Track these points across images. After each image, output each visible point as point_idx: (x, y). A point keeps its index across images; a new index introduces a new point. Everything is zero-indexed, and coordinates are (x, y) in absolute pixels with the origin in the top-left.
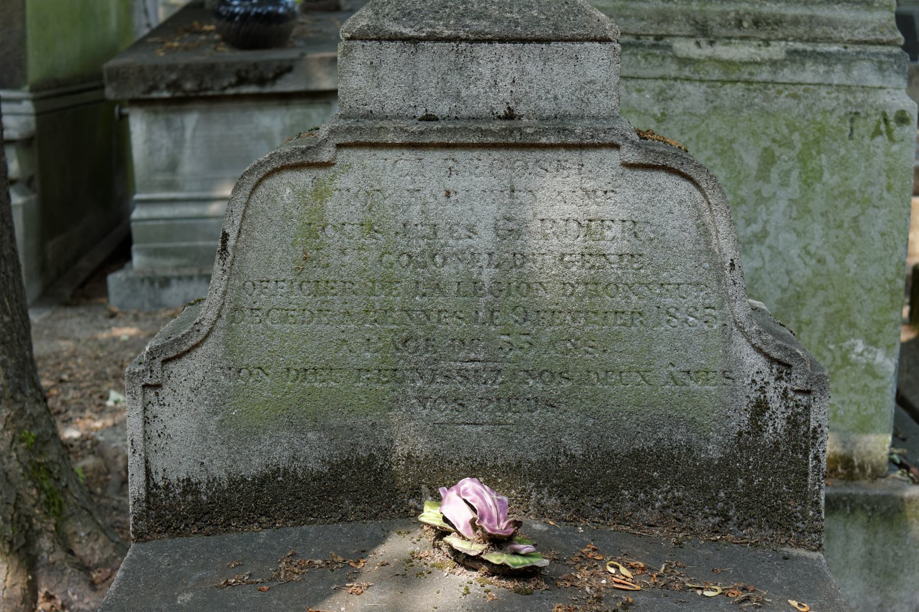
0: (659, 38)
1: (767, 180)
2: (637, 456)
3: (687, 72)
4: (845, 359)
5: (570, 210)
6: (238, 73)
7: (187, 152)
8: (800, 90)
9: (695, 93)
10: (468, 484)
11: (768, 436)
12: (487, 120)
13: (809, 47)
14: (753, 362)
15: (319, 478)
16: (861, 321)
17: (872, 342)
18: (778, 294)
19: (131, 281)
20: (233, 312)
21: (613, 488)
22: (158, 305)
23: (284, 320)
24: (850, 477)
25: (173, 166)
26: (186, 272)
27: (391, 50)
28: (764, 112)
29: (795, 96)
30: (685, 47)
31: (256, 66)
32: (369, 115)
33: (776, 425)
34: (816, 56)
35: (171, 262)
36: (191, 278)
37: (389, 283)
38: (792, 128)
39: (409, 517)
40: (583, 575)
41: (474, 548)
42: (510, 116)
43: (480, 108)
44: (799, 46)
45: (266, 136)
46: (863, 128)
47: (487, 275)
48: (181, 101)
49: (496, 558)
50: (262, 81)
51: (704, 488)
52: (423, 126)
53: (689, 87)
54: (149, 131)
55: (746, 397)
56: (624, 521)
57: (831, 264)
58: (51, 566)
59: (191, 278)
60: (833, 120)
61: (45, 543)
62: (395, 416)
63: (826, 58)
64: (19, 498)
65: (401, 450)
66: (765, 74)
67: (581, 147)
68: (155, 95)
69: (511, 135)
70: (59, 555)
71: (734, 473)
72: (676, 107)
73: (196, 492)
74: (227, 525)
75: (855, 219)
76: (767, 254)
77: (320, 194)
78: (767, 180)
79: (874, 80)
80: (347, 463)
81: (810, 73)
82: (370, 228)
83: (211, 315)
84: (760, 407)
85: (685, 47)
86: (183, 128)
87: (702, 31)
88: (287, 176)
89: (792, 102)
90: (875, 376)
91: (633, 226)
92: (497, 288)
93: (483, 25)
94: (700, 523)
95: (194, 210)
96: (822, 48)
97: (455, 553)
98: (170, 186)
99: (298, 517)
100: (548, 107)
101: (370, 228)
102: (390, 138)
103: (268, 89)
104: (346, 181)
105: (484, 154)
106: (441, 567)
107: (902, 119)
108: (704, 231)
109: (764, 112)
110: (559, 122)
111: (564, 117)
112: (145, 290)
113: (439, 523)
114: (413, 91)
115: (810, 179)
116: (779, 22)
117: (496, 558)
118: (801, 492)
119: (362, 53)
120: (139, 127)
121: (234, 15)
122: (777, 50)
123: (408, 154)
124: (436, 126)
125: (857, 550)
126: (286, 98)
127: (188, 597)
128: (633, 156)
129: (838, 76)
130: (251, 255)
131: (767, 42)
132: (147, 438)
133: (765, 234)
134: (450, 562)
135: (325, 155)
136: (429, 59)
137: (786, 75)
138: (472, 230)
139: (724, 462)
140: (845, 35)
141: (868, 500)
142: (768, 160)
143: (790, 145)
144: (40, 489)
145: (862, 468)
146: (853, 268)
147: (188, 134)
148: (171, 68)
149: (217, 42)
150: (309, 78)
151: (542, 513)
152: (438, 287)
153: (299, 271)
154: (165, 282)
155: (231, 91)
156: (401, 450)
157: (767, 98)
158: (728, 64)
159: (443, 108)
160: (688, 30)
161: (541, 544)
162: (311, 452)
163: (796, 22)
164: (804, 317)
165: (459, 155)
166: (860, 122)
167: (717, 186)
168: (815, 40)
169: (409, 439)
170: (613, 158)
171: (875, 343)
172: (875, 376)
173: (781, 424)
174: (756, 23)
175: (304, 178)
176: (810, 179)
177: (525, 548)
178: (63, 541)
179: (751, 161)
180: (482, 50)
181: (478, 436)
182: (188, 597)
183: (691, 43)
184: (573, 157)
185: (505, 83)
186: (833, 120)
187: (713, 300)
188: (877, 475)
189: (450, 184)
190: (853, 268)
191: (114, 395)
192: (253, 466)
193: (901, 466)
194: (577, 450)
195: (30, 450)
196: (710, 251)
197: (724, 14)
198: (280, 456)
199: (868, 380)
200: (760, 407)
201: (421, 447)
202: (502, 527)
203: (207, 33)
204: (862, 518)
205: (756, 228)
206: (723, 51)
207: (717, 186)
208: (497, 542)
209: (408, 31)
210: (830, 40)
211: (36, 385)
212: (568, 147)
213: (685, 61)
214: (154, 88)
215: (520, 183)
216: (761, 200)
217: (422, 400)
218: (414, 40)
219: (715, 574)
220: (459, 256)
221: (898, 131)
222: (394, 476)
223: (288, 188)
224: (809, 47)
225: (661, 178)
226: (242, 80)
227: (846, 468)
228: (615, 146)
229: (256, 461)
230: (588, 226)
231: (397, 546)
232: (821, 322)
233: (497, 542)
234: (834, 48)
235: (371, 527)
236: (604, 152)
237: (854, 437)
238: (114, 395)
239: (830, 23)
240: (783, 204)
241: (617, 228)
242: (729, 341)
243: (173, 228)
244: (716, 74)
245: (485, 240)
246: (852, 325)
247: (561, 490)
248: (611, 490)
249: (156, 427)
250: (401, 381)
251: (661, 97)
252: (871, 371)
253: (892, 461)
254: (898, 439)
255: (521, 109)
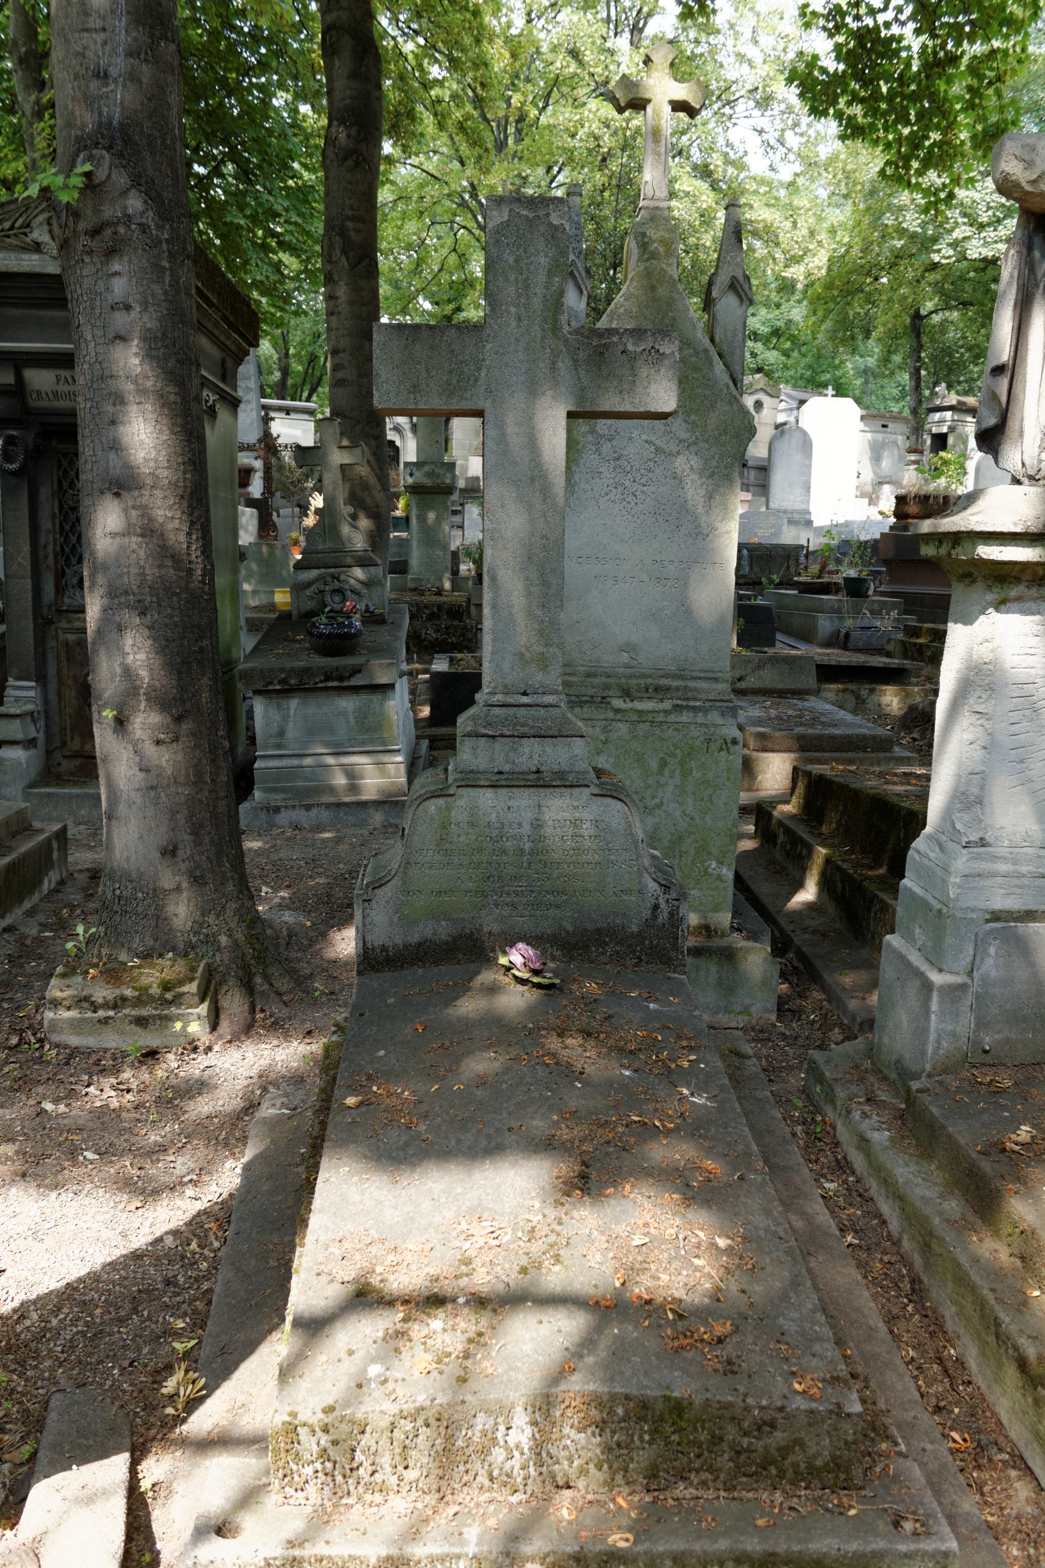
0: (603, 698)
1: (663, 775)
2: (598, 931)
3: (619, 717)
4: (705, 871)
5: (567, 815)
6: (326, 674)
7: (291, 724)
8: (680, 726)
9: (623, 728)
10: (520, 945)
11: (660, 920)
12: (528, 773)
13: (684, 703)
14: (652, 886)
15: (447, 943)
16: (714, 851)
17: (720, 863)
18: (669, 837)
19: (254, 809)
20: (407, 865)
21: (587, 946)
22: (272, 825)
23: (431, 868)
24: (709, 936)
25: (281, 733)
26: (291, 803)
27: (483, 740)
28: (661, 738)
29: (677, 730)
30: (618, 703)
31: (337, 668)
32: (471, 772)
33: (663, 916)
34: (688, 708)
35: (281, 796)
36: (294, 807)
37: (481, 850)
38: (676, 747)
39: (490, 962)
40: (574, 987)
41: (524, 975)
42: (538, 772)
43: (524, 768)
44: (679, 702)
45: (344, 714)
46: (714, 746)
47: (527, 846)
48: (288, 691)
49: (536, 980)
50: (341, 679)
51: (630, 946)
52: (498, 777)
53: (620, 725)
54: (266, 710)
55: (649, 903)
56: (592, 962)
57: (698, 820)
58: (262, 993)
59: (294, 807)
60: (698, 743)
61: (258, 980)
62: (483, 913)
63: (694, 708)
64: (243, 954)
65: (486, 929)
66: (661, 718)
67: (572, 786)
68: (270, 688)
69: (539, 780)
70: (266, 987)
71: (644, 938)
72: (614, 736)
73: (387, 951)
74: (402, 966)
75: (710, 796)
76: (663, 815)
77: (449, 808)
78: (663, 775)
79: (719, 721)
80: (460, 936)
81: (685, 717)
82: (472, 824)
83: (396, 866)
84: (656, 907)
85: (618, 703)
86: (289, 708)
87: (627, 694)
88: (433, 800)
89: (675, 733)
90: (722, 881)
91: (596, 823)
92: (533, 852)
93: (525, 729)
94: (628, 962)
95: (295, 762)
96: (692, 703)
97: (516, 977)
98: (279, 746)
99: (436, 962)
100: (556, 768)
101: (472, 824)
102: (482, 783)
103: (345, 684)
104: (461, 803)
105: (526, 790)
106: (509, 984)
107: (735, 742)
108: (629, 825)
109: (661, 738)
110: (561, 775)
111: (563, 772)
112: (263, 815)
113: (507, 964)
114: (492, 760)
115: (686, 774)
116: (668, 689)
117: (536, 980)
118: (675, 947)
119: (469, 743)
120: (259, 707)
121: (322, 634)
122: (667, 705)
123: (490, 790)
124: (504, 777)
125: (713, 976)
126: (356, 689)
127: (392, 1000)
128: (595, 791)
129: (700, 718)
130: (415, 838)
131: (662, 700)
132: (364, 926)
133: (661, 804)
134: (513, 982)
135: (451, 792)
136: (499, 745)
137: (673, 718)
138: (520, 825)
139: (639, 933)
140: (704, 696)
141: (719, 948)
142: (663, 764)
143: (674, 756)
144: (254, 949)
145: (716, 931)
146: (710, 822)
147: (292, 712)
148: (281, 670)
149: (307, 649)
150: (372, 677)
151: (553, 959)
152: (504, 852)
153: (438, 845)
154: (277, 810)
155: (321, 685)
156: (486, 929)
157: (662, 731)
158: (640, 712)
159: (507, 768)
160: (619, 693)
161: (556, 973)
162: (443, 931)
163: (677, 689)
164: (684, 849)
165: (514, 790)
166: (712, 744)
167: (635, 804)
168: (687, 699)
169: (490, 923)
170: (586, 791)
171: (722, 863)
172: (722, 881)
173: (666, 915)
174: (656, 690)
175: (441, 801)
176: (686, 774)
177: (549, 975)
178: (266, 977)
179: (654, 765)
180: (525, 741)
181: (522, 922)
182: (392, 1000)
183: (621, 701)
184: (569, 790)
185: (536, 757)
186: (698, 743)
187: (634, 857)
188: (723, 935)
189: (510, 803)
190: (710, 822)
191: (264, 889)
192: (415, 938)
193: (739, 930)
194: (570, 928)
195: (248, 927)
196: (631, 834)
197: (639, 685)
198: (428, 933)
199: (718, 883)
200: (656, 907)
201: (496, 928)
202: (537, 966)
203: (299, 641)
204: (715, 959)
205: (657, 801)
206: (638, 705)
207: (635, 804)
208: (536, 972)
209: (490, 733)
210: (696, 699)
211: (248, 889)
212: (565, 786)
213: (617, 711)
214: (270, 683)
215: (542, 803)
216: (659, 785)
217: (497, 906)
218: (493, 737)
219: (634, 986)
220: (514, 837)
221: (732, 749)
222: (483, 942)
223: (433, 806)
224: (684, 703)
225: (609, 800)
226: (328, 678)
227: (706, 930)
228: (587, 786)
229: (416, 936)
230: (576, 823)
231: (486, 977)
232: (692, 852)
233: (536, 972)
234: (698, 704)
235: (472, 967)
236: (582, 789)
237: (711, 914)
238: (264, 889)
239: (696, 690)
240: (671, 788)
241: (588, 824)
242: (641, 876)
243: (282, 774)
244: (635, 717)
245: (526, 829)
246: (709, 853)
247: (562, 947)
248: (586, 947)
249: (369, 920)
250: (486, 897)
251: (605, 730)
252: (719, 878)
253: (732, 927)
254: (736, 913)
255: (543, 769)
